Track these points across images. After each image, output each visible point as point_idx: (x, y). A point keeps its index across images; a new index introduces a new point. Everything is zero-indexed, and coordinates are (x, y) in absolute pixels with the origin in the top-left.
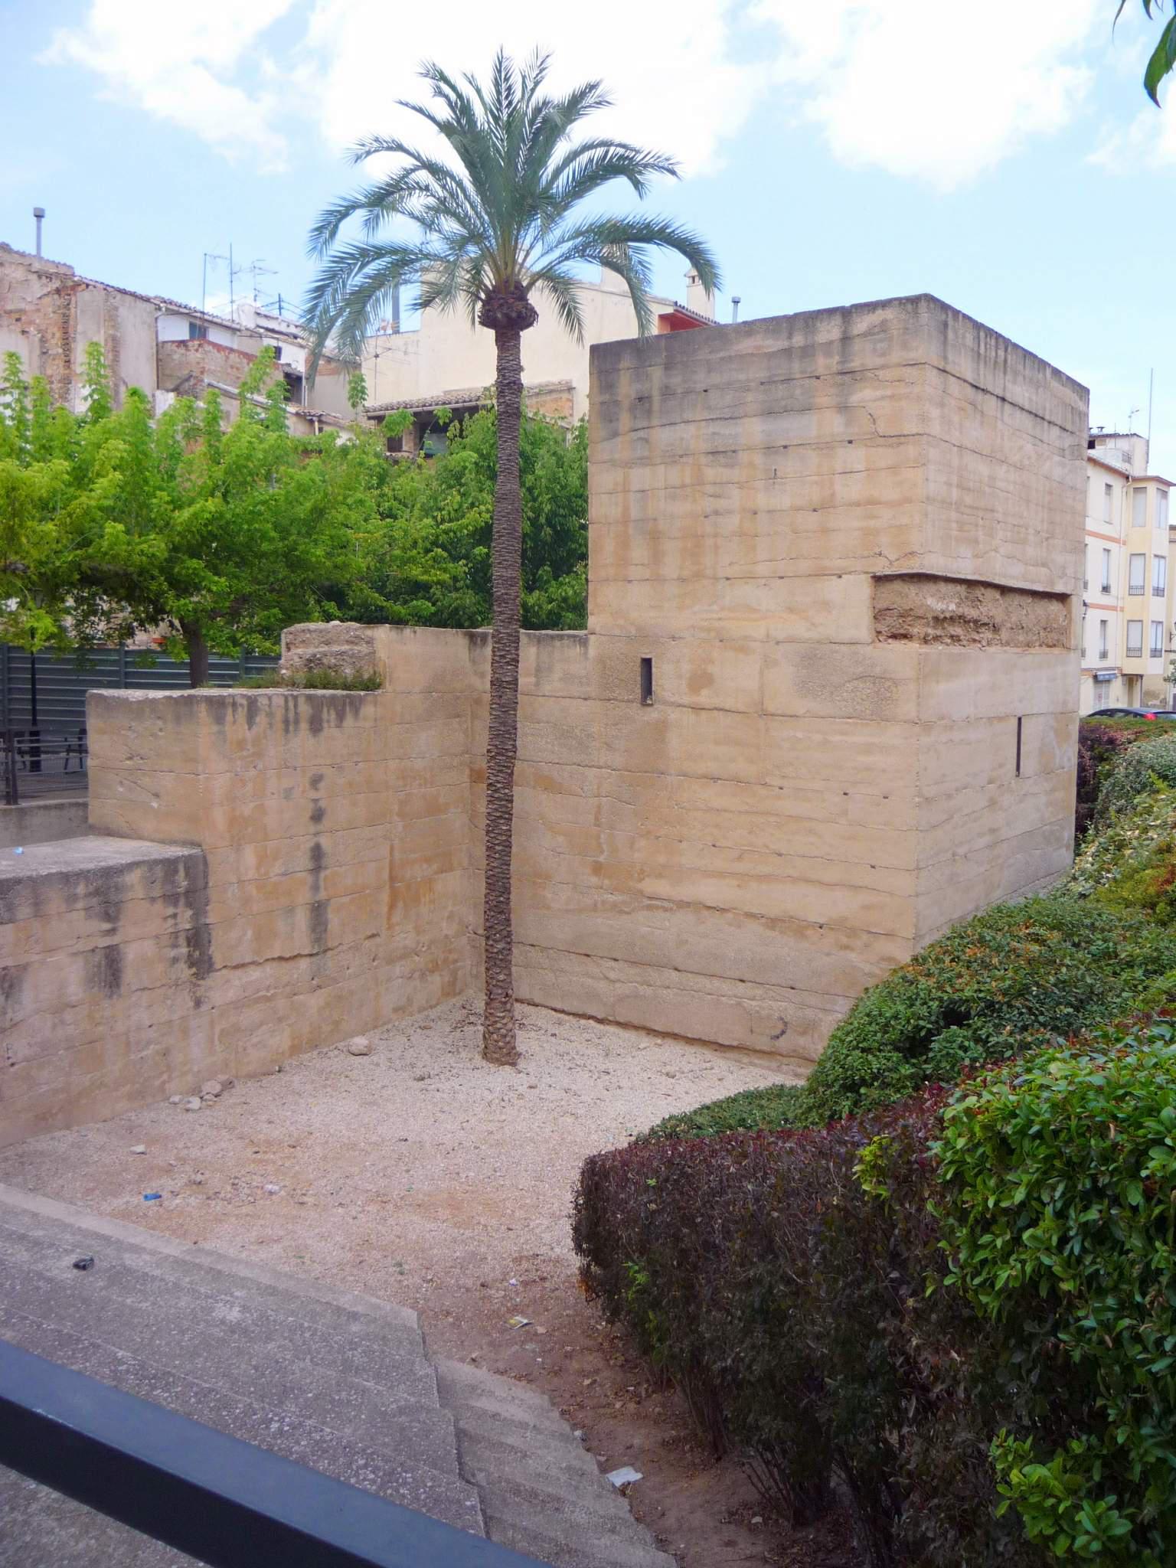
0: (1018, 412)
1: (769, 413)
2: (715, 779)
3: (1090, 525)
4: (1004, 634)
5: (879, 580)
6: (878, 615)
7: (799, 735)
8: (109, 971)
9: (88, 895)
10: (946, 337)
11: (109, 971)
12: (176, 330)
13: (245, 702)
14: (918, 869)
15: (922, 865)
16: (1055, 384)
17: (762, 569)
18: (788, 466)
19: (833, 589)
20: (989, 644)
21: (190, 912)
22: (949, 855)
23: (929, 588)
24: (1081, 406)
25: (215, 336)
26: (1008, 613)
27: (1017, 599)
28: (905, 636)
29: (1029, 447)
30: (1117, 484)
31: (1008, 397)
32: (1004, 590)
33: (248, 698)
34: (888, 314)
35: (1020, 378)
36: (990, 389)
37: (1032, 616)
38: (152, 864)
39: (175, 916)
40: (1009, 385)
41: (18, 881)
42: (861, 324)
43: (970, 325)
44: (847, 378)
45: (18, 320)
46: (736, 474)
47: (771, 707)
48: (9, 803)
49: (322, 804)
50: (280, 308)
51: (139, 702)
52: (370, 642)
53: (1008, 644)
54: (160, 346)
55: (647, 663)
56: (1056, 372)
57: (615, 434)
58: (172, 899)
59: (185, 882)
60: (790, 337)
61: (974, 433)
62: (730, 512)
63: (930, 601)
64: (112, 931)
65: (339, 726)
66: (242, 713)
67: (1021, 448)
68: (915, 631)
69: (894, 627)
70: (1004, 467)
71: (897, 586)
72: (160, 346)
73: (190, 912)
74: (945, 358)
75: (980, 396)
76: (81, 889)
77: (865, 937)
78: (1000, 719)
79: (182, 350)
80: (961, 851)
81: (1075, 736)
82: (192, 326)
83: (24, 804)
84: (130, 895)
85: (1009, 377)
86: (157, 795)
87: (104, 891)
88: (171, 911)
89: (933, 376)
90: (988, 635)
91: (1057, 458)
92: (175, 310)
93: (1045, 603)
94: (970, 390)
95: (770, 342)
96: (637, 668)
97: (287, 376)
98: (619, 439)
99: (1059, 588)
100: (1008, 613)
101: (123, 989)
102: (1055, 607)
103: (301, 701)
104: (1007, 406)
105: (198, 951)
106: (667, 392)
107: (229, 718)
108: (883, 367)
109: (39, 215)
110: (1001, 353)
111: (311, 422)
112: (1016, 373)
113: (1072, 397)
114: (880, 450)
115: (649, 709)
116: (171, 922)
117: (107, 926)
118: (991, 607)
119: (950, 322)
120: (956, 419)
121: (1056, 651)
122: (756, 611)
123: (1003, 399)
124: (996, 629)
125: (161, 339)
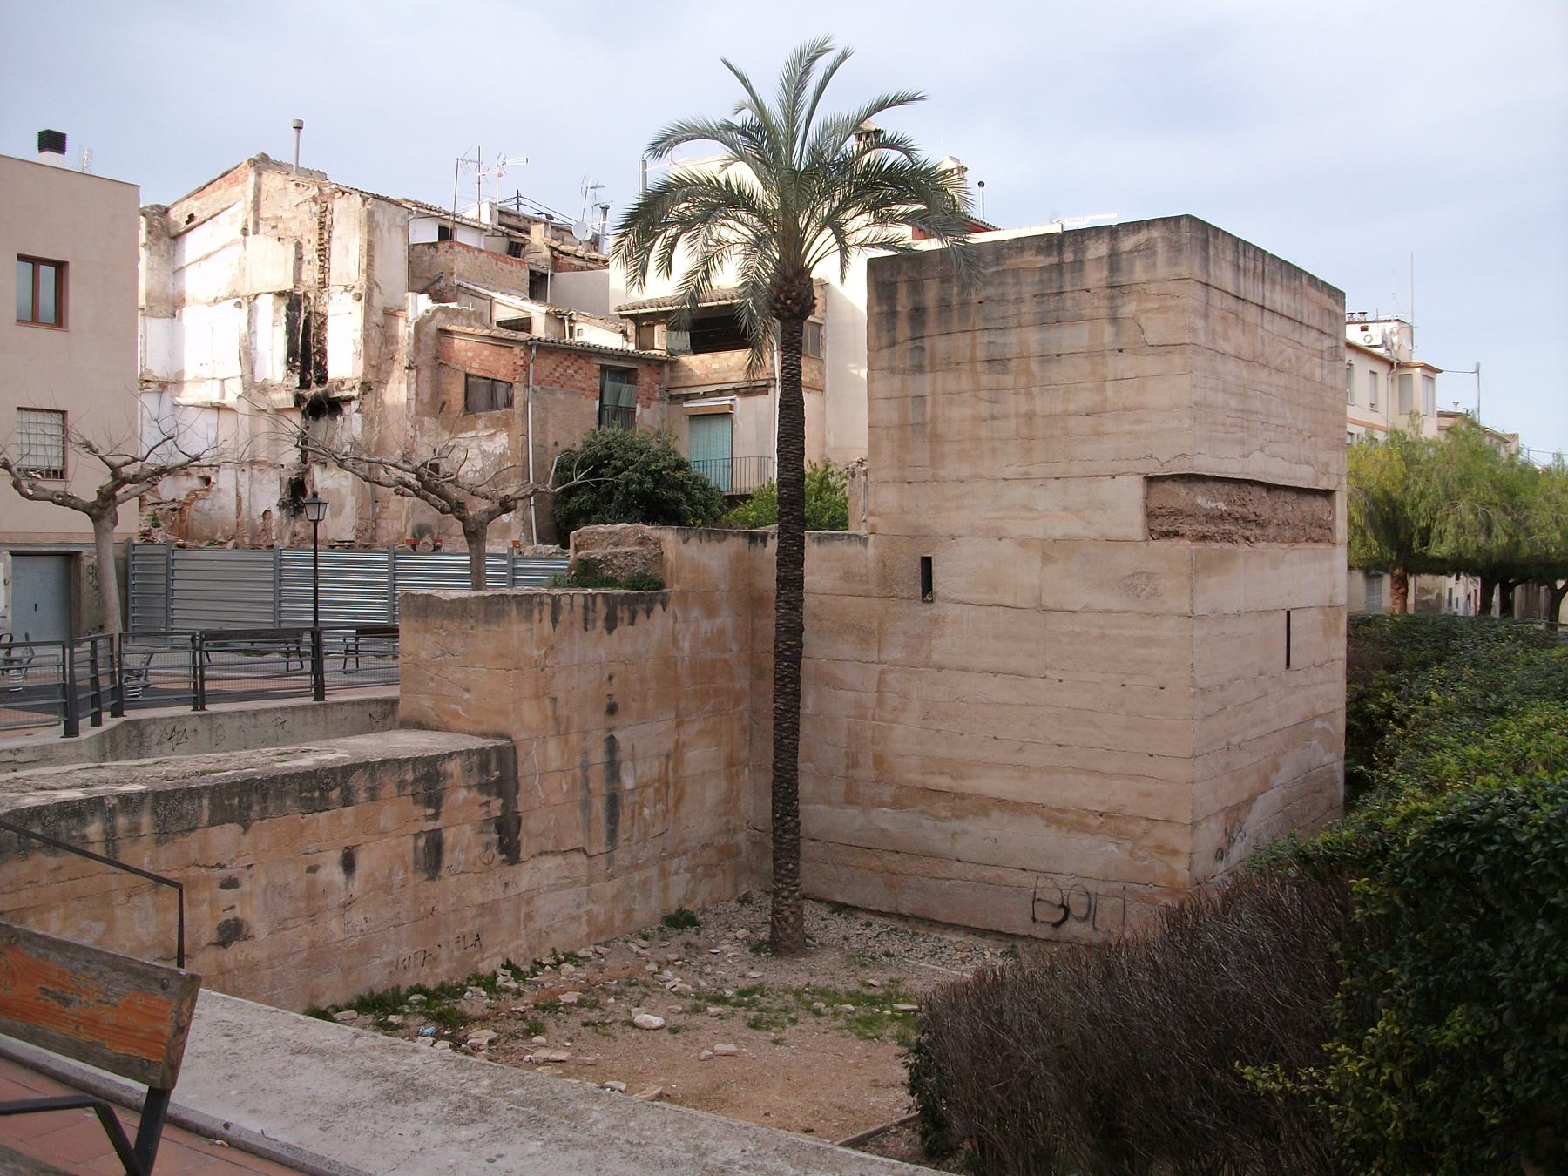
0: (1277, 318)
1: (1043, 323)
2: (996, 673)
3: (1351, 412)
4: (1272, 531)
5: (1150, 480)
6: (1150, 515)
7: (1078, 629)
8: (432, 855)
9: (416, 781)
10: (1207, 253)
11: (432, 855)
12: (426, 233)
13: (549, 601)
14: (1194, 756)
15: (1198, 753)
16: (1312, 292)
17: (1036, 470)
18: (1058, 373)
19: (1107, 488)
20: (1257, 539)
21: (500, 801)
22: (1223, 744)
23: (1199, 488)
24: (1338, 309)
25: (462, 236)
26: (1274, 510)
27: (1284, 496)
28: (1176, 534)
29: (1290, 351)
30: (1382, 370)
31: (1267, 304)
32: (1270, 488)
33: (553, 597)
34: (1155, 233)
35: (1278, 287)
36: (1250, 298)
37: (1298, 512)
38: (469, 752)
39: (487, 803)
40: (1267, 294)
41: (193, 793)
42: (1127, 243)
43: (1230, 241)
44: (1115, 291)
45: (274, 227)
46: (1008, 380)
47: (1049, 602)
48: (195, 709)
49: (616, 699)
50: (518, 204)
51: (453, 601)
52: (658, 543)
53: (1275, 540)
54: (412, 248)
55: (927, 563)
56: (1311, 278)
57: (893, 343)
58: (483, 788)
59: (498, 770)
60: (1060, 253)
61: (1236, 340)
62: (1006, 417)
63: (1200, 500)
64: (436, 817)
65: (632, 623)
66: (547, 610)
67: (1281, 352)
68: (1185, 529)
69: (1161, 524)
70: (1266, 371)
71: (1168, 485)
72: (412, 248)
73: (500, 801)
74: (1208, 272)
75: (1240, 306)
76: (410, 776)
77: (1144, 823)
78: (1267, 612)
79: (432, 251)
80: (1235, 740)
81: (1343, 628)
82: (441, 228)
83: (211, 708)
84: (449, 783)
85: (1267, 286)
86: (468, 690)
87: (427, 779)
88: (485, 798)
89: (1199, 291)
90: (1257, 531)
91: (1318, 360)
92: (426, 212)
93: (1309, 499)
94: (1231, 302)
95: (1041, 258)
96: (917, 567)
97: (532, 273)
98: (897, 347)
99: (1323, 485)
100: (1274, 510)
101: (443, 872)
102: (1319, 503)
103: (599, 600)
104: (1266, 313)
105: (507, 839)
106: (945, 305)
107: (536, 616)
108: (1148, 282)
109: (299, 128)
110: (1260, 265)
111: (562, 320)
112: (1273, 282)
113: (1330, 303)
114: (1149, 359)
115: (927, 606)
116: (485, 809)
117: (430, 811)
118: (1261, 505)
119: (1211, 239)
120: (1219, 328)
121: (1321, 546)
122: (1031, 509)
123: (1263, 307)
124: (1260, 525)
125: (412, 242)
